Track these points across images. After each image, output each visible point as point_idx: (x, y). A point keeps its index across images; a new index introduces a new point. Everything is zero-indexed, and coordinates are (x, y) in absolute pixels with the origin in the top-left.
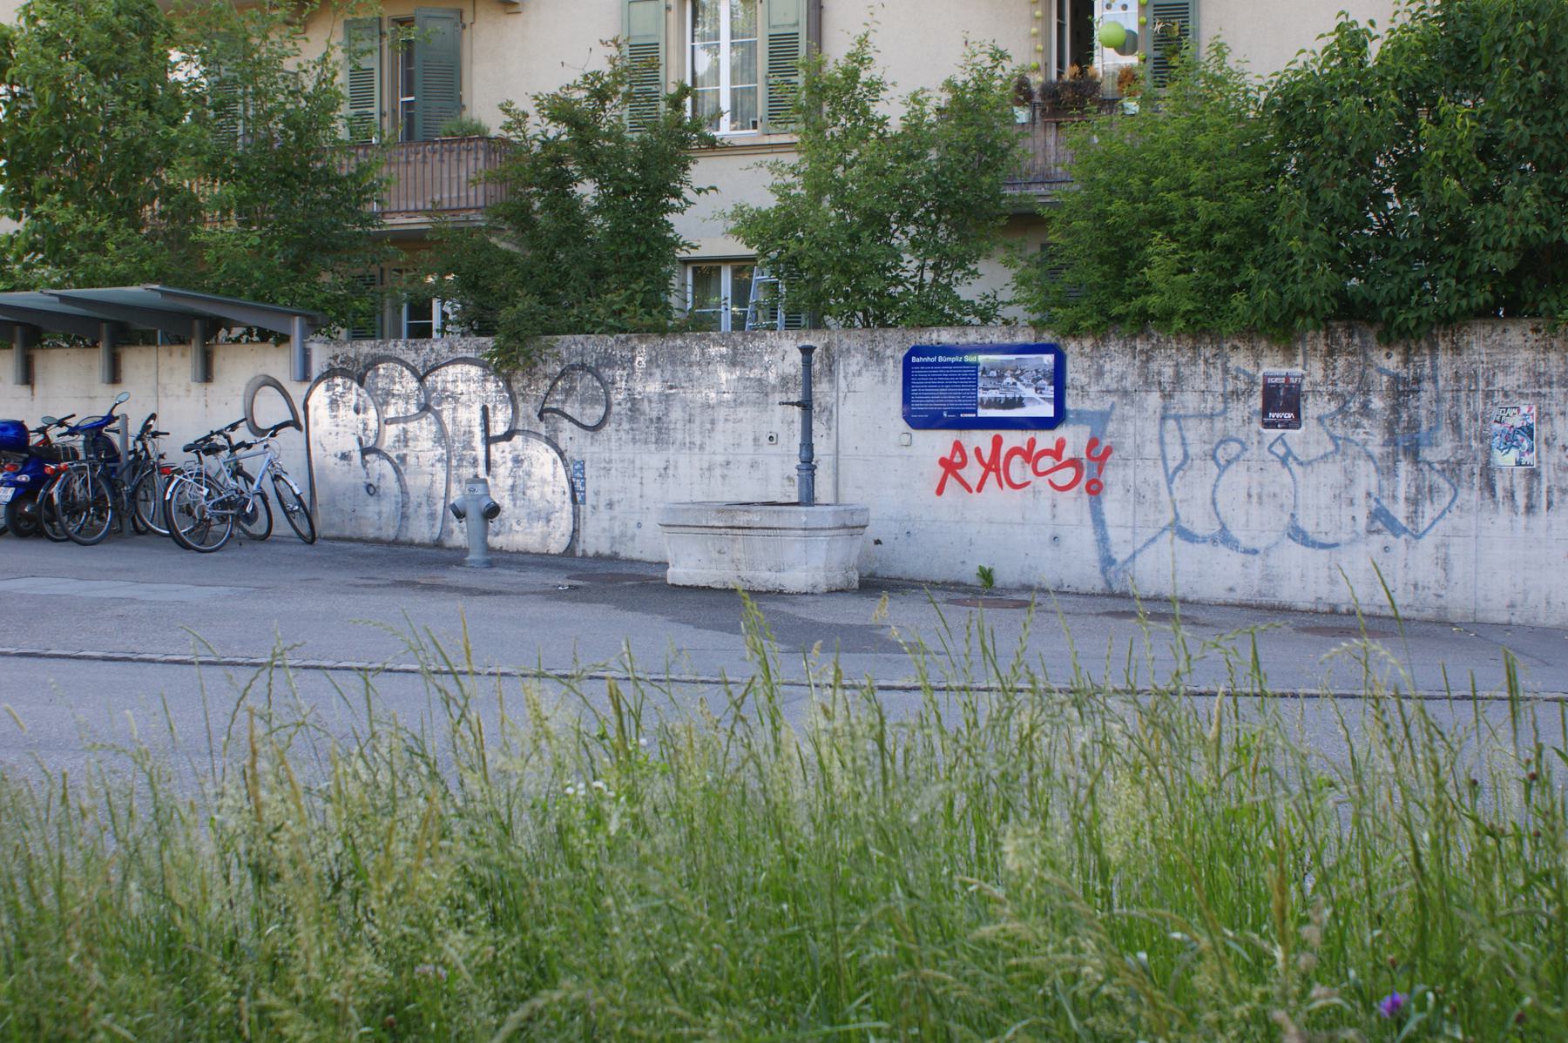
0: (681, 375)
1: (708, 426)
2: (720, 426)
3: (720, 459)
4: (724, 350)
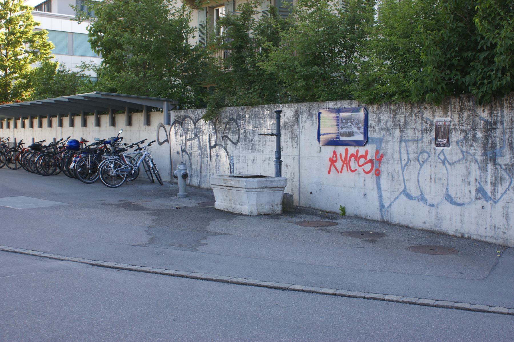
0: (257, 122)
1: (265, 143)
2: (268, 143)
3: (268, 156)
4: (269, 112)
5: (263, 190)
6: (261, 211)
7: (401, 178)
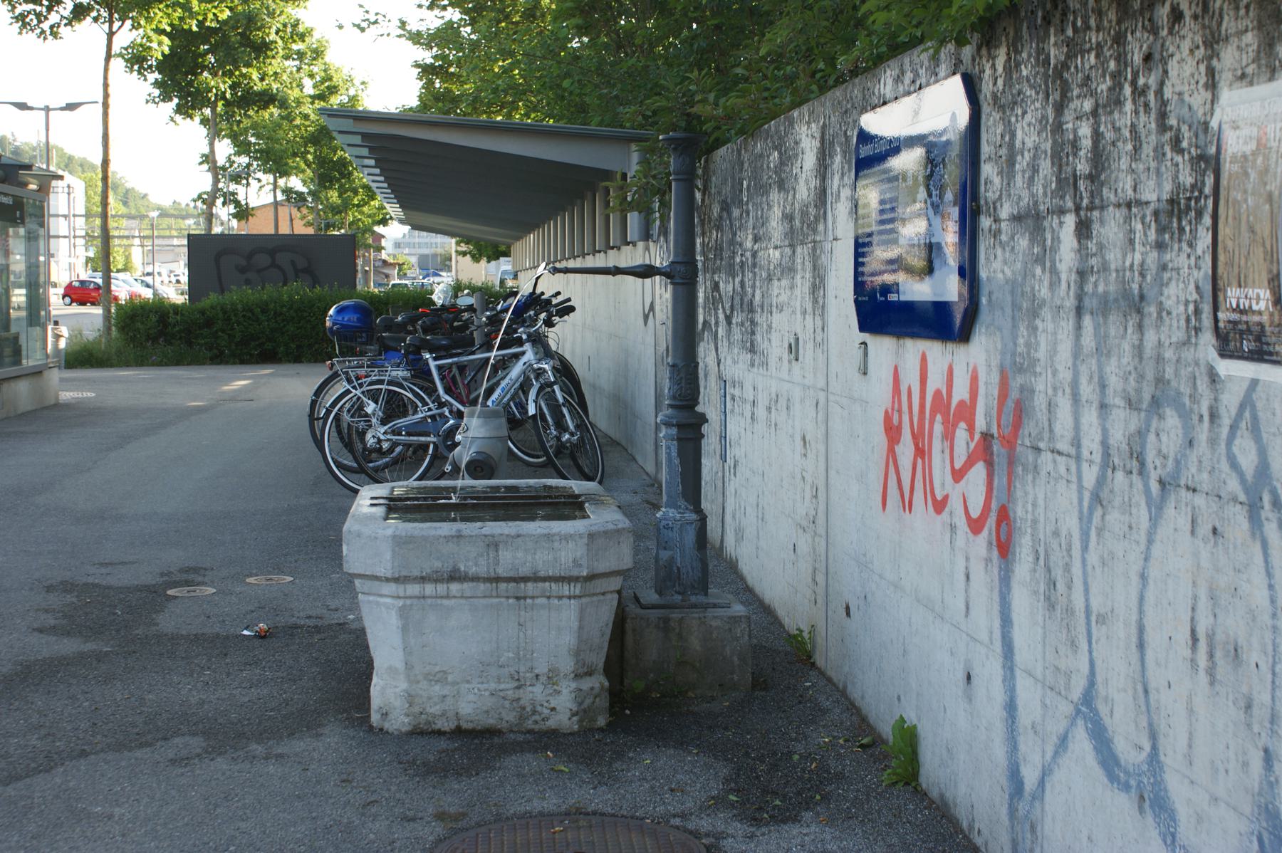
5: (441, 588)
6: (436, 710)
7: (1079, 604)
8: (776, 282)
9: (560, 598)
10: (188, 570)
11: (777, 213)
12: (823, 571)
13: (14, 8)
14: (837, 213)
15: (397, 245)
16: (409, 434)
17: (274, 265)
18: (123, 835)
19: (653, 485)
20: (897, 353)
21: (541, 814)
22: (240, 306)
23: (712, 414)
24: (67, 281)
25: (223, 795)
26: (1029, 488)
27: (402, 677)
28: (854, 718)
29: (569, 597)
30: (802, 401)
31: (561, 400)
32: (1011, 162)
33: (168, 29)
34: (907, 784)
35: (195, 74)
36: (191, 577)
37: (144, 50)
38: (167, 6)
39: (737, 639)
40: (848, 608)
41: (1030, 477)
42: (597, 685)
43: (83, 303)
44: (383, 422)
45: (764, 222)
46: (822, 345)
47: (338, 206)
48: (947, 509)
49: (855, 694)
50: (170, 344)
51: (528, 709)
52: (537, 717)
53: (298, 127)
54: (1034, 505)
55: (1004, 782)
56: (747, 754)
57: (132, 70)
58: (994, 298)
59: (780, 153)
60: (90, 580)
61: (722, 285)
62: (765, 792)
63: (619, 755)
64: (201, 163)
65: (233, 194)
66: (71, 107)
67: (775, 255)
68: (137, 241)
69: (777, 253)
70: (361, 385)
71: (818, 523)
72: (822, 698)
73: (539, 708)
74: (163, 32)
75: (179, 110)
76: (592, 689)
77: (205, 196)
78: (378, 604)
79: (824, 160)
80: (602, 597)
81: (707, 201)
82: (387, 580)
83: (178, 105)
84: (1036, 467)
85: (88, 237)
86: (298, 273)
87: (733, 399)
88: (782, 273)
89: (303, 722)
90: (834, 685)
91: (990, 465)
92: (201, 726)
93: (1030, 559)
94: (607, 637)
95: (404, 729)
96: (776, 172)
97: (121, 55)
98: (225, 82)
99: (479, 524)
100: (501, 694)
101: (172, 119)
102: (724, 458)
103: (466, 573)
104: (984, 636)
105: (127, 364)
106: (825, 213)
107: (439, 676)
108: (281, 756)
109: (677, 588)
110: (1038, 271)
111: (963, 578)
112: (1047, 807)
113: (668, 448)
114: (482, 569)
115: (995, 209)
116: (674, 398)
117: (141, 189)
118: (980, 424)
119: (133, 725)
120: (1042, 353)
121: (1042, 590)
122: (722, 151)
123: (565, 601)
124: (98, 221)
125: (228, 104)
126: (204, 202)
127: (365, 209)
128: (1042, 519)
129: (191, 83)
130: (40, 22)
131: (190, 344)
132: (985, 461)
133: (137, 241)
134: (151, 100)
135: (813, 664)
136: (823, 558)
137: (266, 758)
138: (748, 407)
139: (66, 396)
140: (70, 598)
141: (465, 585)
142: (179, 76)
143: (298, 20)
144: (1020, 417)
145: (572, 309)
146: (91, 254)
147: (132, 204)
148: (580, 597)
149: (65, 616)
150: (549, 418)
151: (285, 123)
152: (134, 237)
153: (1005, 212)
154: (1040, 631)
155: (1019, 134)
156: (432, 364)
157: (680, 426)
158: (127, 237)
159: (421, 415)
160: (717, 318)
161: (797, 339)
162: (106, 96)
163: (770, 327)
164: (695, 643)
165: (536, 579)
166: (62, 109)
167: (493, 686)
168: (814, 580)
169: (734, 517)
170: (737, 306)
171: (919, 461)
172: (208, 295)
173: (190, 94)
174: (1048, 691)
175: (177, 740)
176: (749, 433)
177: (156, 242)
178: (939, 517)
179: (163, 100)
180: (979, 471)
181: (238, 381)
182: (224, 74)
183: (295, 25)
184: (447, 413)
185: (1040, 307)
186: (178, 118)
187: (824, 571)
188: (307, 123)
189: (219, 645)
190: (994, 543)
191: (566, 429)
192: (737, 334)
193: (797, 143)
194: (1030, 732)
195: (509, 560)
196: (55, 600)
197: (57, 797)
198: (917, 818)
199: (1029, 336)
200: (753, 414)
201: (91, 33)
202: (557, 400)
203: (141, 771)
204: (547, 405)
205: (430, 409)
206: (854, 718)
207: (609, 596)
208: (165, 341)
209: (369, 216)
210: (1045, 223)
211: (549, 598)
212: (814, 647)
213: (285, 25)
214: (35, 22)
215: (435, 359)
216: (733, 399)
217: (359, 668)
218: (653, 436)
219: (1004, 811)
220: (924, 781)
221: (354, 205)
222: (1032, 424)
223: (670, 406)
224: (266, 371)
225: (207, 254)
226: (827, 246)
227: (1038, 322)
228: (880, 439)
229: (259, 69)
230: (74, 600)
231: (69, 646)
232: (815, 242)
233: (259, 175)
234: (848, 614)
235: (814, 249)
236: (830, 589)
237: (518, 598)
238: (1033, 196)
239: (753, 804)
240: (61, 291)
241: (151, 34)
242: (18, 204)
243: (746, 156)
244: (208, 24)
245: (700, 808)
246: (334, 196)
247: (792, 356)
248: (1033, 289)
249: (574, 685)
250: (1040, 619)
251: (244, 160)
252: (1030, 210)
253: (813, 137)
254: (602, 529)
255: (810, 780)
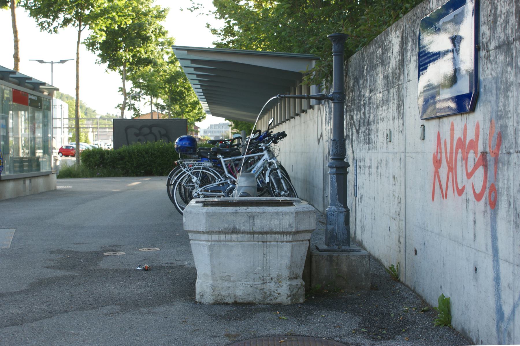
5: (228, 237)
6: (225, 293)
8: (380, 109)
9: (282, 242)
10: (113, 246)
11: (381, 76)
12: (403, 238)
13: (38, 20)
14: (409, 69)
15: (205, 132)
16: (211, 192)
17: (151, 133)
18: (84, 341)
19: (322, 216)
20: (439, 126)
21: (274, 335)
22: (136, 151)
23: (350, 162)
24: (60, 147)
25: (128, 327)
26: (506, 173)
27: (210, 278)
28: (419, 301)
29: (287, 242)
30: (393, 160)
31: (280, 176)
32: (495, 22)
33: (105, 29)
34: (445, 325)
35: (116, 51)
36: (114, 248)
37: (94, 38)
38: (105, 19)
39: (364, 266)
40: (416, 251)
41: (506, 167)
42: (299, 283)
43: (67, 156)
44: (200, 186)
45: (374, 82)
46: (402, 132)
47: (179, 112)
48: (464, 193)
49: (419, 290)
50: (106, 168)
51: (268, 294)
52: (272, 297)
53: (162, 76)
54: (508, 180)
55: (494, 315)
56: (369, 314)
57: (89, 49)
58: (487, 88)
59: (382, 49)
60: (70, 249)
61: (354, 117)
62: (378, 328)
63: (310, 313)
64: (119, 91)
65: (133, 105)
66: (62, 62)
67: (380, 96)
68: (91, 130)
69: (381, 95)
70: (190, 170)
71: (401, 216)
72: (404, 293)
73: (273, 293)
74: (103, 30)
75: (110, 67)
76: (297, 285)
77: (121, 106)
78: (199, 244)
79: (403, 46)
80: (301, 242)
81: (347, 80)
82: (204, 233)
83: (109, 65)
84: (508, 162)
85: (70, 128)
86: (162, 136)
87: (360, 167)
88: (383, 104)
89: (167, 300)
90: (409, 288)
91: (486, 166)
92: (119, 302)
93: (506, 206)
94: (304, 261)
95: (211, 302)
96: (380, 58)
97: (84, 43)
98: (129, 54)
99: (245, 208)
100: (255, 286)
101: (106, 71)
102: (356, 195)
103: (239, 230)
104: (483, 248)
105: (86, 176)
106: (404, 70)
107: (227, 278)
108: (155, 313)
109: (336, 243)
110: (509, 69)
111: (472, 223)
112: (516, 323)
113: (331, 178)
114: (246, 228)
115: (487, 46)
116: (334, 155)
117: (93, 108)
118: (480, 148)
119: (88, 301)
120: (511, 108)
121: (512, 219)
122: (355, 56)
123: (285, 243)
124: (74, 122)
125: (131, 64)
126: (120, 108)
127: (191, 114)
128: (512, 186)
129: (115, 55)
130: (49, 26)
131: (114, 168)
132: (483, 165)
133: (91, 130)
134: (97, 62)
135: (399, 280)
136: (404, 230)
137: (148, 313)
138: (367, 169)
139: (59, 187)
140: (60, 256)
141: (239, 236)
142: (109, 52)
143: (161, 27)
144: (501, 140)
145: (286, 135)
146: (71, 136)
147: (88, 115)
148: (292, 242)
149: (58, 262)
150: (275, 184)
151: (156, 73)
152: (89, 128)
153: (492, 46)
154: (511, 239)
155: (499, 8)
156: (222, 160)
157: (337, 168)
158: (87, 128)
159: (217, 183)
160: (352, 132)
161: (391, 132)
162: (78, 58)
163: (378, 130)
164: (344, 268)
165: (271, 233)
166: (58, 63)
167: (251, 283)
168: (399, 241)
169: (361, 221)
170: (362, 124)
171: (450, 173)
172: (122, 146)
173: (114, 60)
174: (516, 267)
175: (108, 307)
176: (368, 181)
177: (99, 130)
178: (460, 197)
179: (103, 63)
180: (481, 170)
181: (135, 183)
182: (129, 51)
183: (160, 29)
184: (229, 182)
185: (510, 86)
186: (109, 70)
187: (404, 236)
188: (166, 74)
189: (127, 273)
190: (488, 203)
191: (282, 189)
192: (362, 137)
193: (390, 42)
194: (507, 288)
195: (259, 224)
196: (54, 256)
197: (54, 327)
198: (451, 339)
199: (505, 101)
200: (370, 172)
201: (72, 30)
202: (278, 176)
203: (92, 318)
204: (274, 178)
205: (221, 180)
206: (419, 301)
207: (305, 242)
208: (103, 166)
209: (193, 117)
210: (513, 46)
211: (277, 242)
212: (399, 273)
213: (156, 29)
214: (47, 26)
215: (224, 158)
216: (360, 167)
217: (192, 275)
218: (322, 193)
219: (494, 329)
220: (453, 324)
221: (186, 112)
222: (506, 142)
223: (332, 159)
224: (147, 179)
225: (121, 128)
226: (405, 86)
227: (510, 94)
228: (431, 167)
229: (144, 49)
230: (63, 256)
231: (60, 273)
232: (399, 85)
233: (144, 96)
234: (416, 253)
235: (398, 89)
236: (407, 244)
237: (263, 242)
238: (506, 34)
239: (373, 332)
240: (58, 151)
241: (98, 31)
242: (39, 99)
243: (366, 55)
244: (122, 26)
245: (348, 334)
246: (177, 107)
247: (388, 140)
248: (506, 78)
249: (289, 283)
250: (512, 233)
251: (138, 90)
252: (504, 42)
253: (398, 37)
254: (302, 210)
255: (399, 324)
